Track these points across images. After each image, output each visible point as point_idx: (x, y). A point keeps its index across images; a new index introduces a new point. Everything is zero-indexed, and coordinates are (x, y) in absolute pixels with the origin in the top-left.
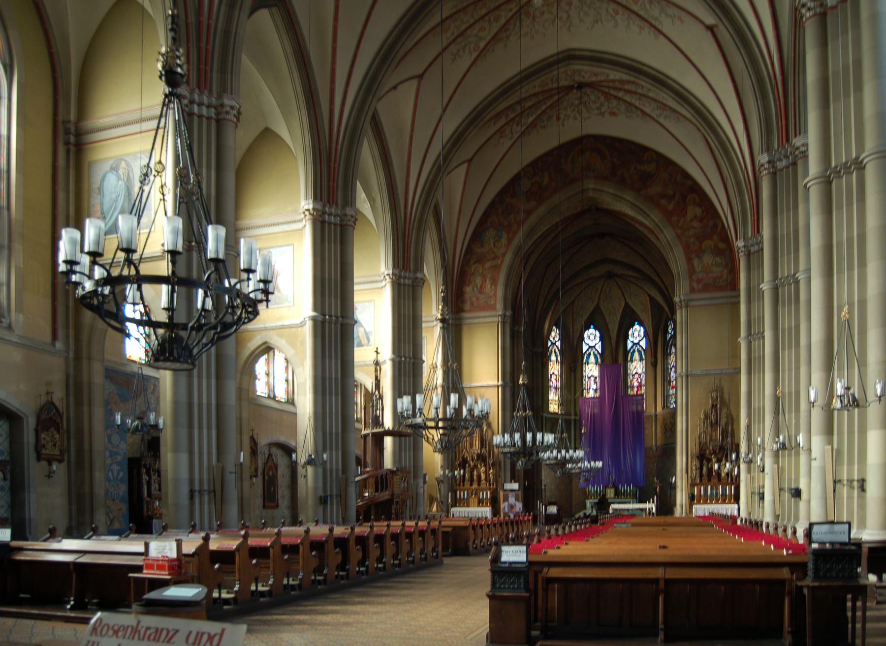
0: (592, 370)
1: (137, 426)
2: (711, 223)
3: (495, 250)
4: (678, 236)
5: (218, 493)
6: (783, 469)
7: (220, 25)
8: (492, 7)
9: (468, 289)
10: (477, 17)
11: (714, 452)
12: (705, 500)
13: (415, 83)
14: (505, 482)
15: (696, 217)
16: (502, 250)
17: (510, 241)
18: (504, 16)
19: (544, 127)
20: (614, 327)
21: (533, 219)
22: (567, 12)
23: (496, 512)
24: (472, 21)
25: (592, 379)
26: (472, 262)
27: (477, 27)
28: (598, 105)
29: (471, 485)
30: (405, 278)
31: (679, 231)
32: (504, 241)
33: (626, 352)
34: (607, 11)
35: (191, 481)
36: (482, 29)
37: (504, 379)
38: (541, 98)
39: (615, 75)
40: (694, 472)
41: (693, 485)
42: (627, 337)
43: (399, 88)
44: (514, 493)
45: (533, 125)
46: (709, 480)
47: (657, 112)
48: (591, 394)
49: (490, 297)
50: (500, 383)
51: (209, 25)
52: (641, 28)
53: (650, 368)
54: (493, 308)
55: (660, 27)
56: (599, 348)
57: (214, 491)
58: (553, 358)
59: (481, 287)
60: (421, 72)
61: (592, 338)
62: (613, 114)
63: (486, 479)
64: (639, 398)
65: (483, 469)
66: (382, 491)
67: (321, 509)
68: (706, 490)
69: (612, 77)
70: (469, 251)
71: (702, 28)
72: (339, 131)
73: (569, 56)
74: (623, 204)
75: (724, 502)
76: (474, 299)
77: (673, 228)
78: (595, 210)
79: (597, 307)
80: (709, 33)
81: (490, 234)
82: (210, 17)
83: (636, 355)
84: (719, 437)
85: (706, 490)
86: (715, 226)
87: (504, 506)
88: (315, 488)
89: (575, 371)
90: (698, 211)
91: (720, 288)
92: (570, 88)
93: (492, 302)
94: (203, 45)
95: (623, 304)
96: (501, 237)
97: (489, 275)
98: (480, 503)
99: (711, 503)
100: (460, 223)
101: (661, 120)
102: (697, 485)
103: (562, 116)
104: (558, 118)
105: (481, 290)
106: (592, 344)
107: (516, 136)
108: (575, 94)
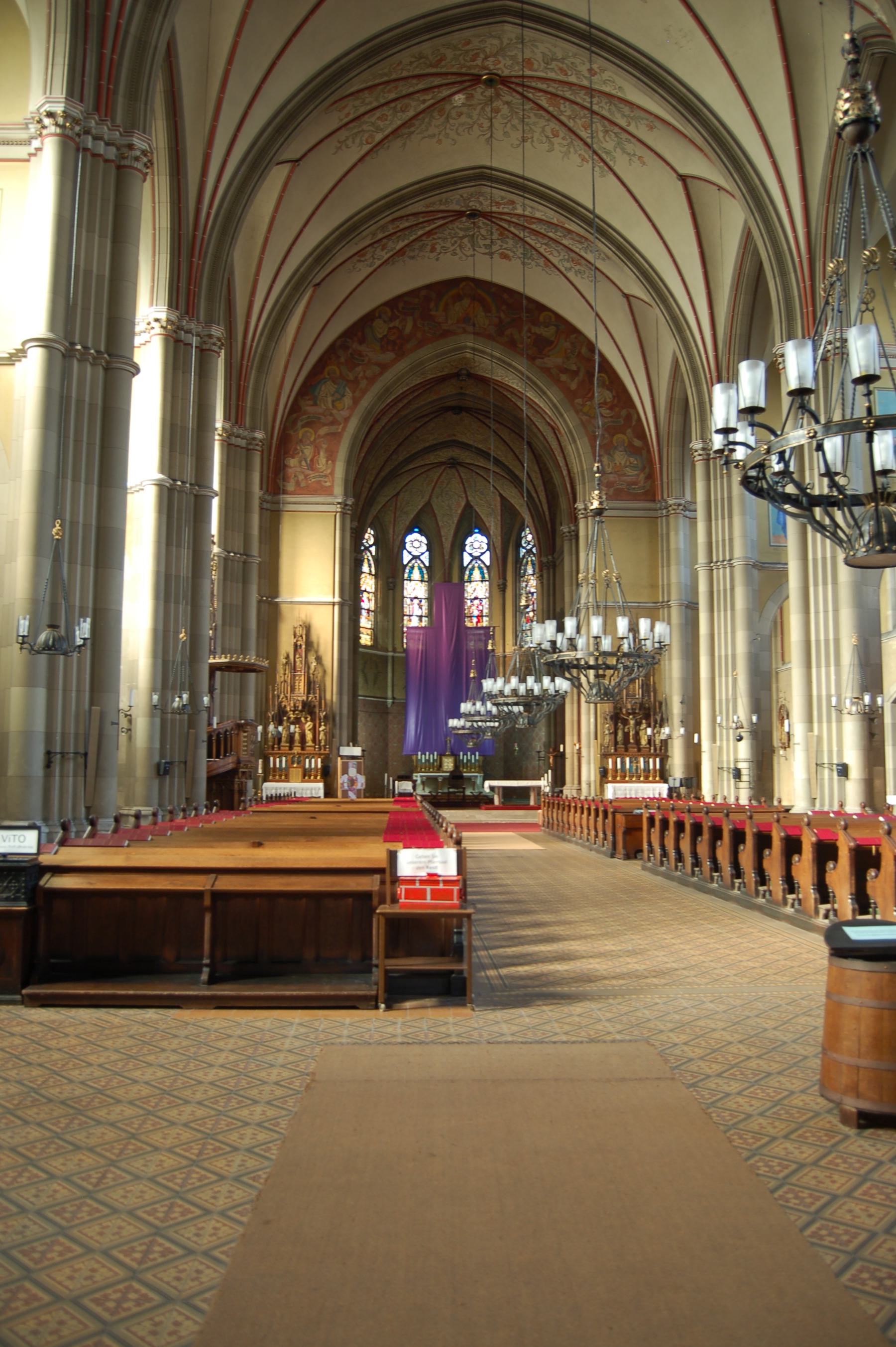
0: (415, 589)
1: (46, 641)
2: (624, 413)
3: (334, 411)
4: (583, 424)
5: (92, 757)
6: (819, 738)
7: (133, 30)
8: (404, 93)
9: (292, 462)
10: (383, 101)
11: (634, 713)
12: (623, 776)
13: (289, 165)
14: (341, 745)
15: (605, 403)
16: (345, 413)
17: (356, 402)
18: (415, 106)
19: (413, 258)
20: (448, 533)
21: (389, 376)
22: (491, 120)
23: (329, 792)
24: (375, 104)
25: (416, 601)
26: (300, 424)
27: (378, 113)
28: (488, 242)
29: (291, 748)
30: (238, 436)
31: (584, 418)
32: (347, 401)
33: (463, 569)
34: (543, 131)
35: (49, 736)
36: (382, 118)
37: (342, 595)
38: (421, 220)
39: (543, 212)
40: (607, 739)
41: (605, 756)
42: (463, 549)
43: (723, 192)
44: (355, 761)
45: (401, 252)
46: (626, 750)
47: (568, 265)
48: (415, 622)
49: (326, 476)
50: (337, 599)
51: (118, 25)
52: (584, 159)
53: (496, 591)
54: (329, 491)
55: (611, 164)
56: (426, 558)
57: (86, 755)
58: (530, 570)
59: (312, 460)
60: (298, 156)
61: (416, 544)
62: (505, 256)
63: (314, 740)
64: (487, 633)
65: (309, 725)
66: (225, 756)
67: (156, 783)
68: (623, 763)
69: (519, 211)
70: (295, 408)
71: (675, 175)
72: (209, 214)
73: (482, 176)
74: (511, 375)
75: (646, 780)
76: (301, 477)
77: (577, 412)
78: (465, 375)
79: (428, 504)
80: (679, 184)
81: (326, 389)
82: (120, 16)
83: (476, 575)
84: (639, 693)
85: (623, 763)
86: (629, 418)
87: (342, 780)
88: (150, 750)
89: (393, 589)
90: (608, 395)
91: (635, 497)
92: (460, 214)
93: (328, 484)
94: (108, 52)
95: (463, 503)
96: (343, 396)
97: (325, 446)
98: (306, 775)
99: (630, 782)
100: (290, 366)
101: (571, 275)
102: (611, 755)
103: (438, 247)
104: (433, 249)
105: (312, 466)
106: (416, 553)
107: (378, 263)
108: (465, 222)
